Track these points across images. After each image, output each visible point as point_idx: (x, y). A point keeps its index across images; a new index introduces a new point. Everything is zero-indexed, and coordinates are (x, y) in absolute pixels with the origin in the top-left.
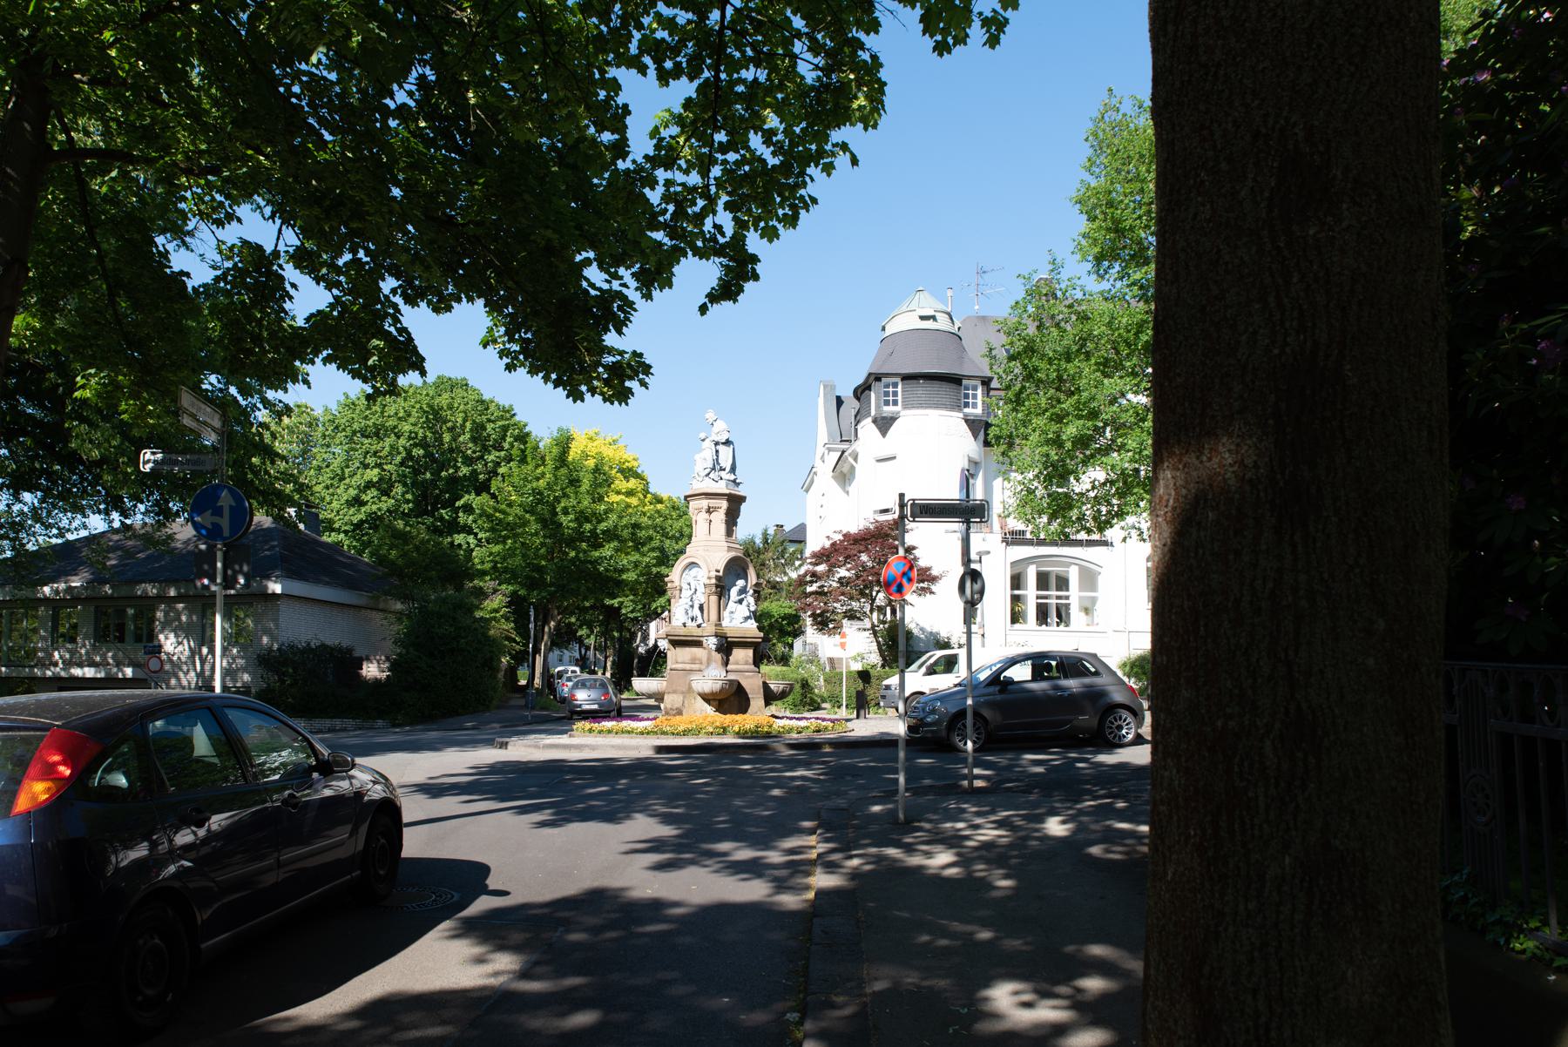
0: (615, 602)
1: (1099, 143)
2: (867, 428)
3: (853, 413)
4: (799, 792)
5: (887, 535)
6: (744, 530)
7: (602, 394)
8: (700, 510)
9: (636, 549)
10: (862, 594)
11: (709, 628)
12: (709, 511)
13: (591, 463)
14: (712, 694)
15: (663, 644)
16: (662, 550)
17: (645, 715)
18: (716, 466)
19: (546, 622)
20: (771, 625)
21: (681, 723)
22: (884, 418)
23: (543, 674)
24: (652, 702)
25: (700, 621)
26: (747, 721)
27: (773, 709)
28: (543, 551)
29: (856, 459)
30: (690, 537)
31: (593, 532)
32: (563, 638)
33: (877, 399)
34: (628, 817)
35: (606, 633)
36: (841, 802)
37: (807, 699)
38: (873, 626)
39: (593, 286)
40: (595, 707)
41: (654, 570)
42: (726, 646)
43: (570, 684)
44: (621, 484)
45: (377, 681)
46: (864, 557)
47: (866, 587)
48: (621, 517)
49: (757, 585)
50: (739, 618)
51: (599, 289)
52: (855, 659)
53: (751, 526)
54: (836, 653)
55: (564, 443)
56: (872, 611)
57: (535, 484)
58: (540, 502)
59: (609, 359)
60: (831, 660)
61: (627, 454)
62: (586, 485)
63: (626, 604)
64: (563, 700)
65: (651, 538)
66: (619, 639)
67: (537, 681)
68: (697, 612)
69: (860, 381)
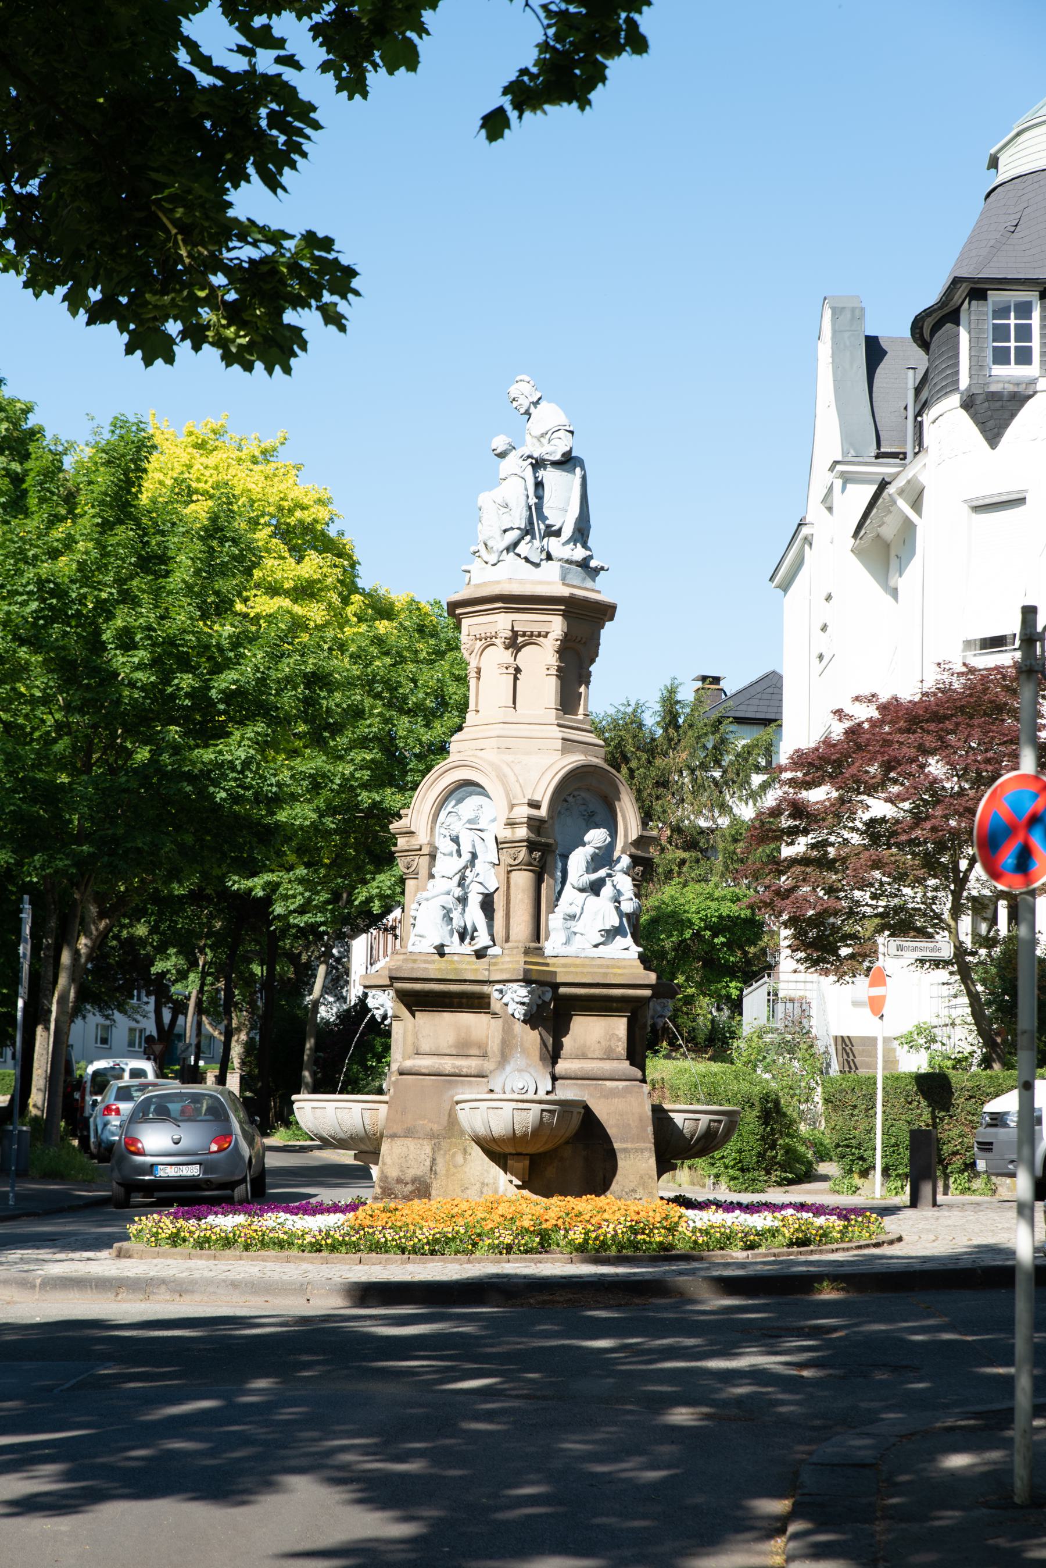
0: (257, 885)
2: (949, 423)
3: (911, 380)
4: (745, 1416)
5: (1000, 708)
6: (607, 693)
7: (221, 343)
8: (488, 641)
9: (317, 740)
10: (931, 865)
11: (508, 960)
12: (515, 643)
13: (199, 511)
14: (514, 1138)
15: (382, 1003)
16: (387, 743)
17: (326, 1195)
18: (535, 524)
19: (65, 938)
20: (682, 948)
21: (423, 1218)
22: (993, 396)
23: (52, 1080)
24: (346, 1157)
25: (483, 939)
26: (607, 1213)
27: (684, 1180)
28: (61, 746)
29: (917, 504)
30: (463, 708)
31: (199, 695)
32: (115, 980)
33: (975, 345)
34: (267, 1484)
35: (229, 968)
36: (858, 1444)
37: (771, 1146)
38: (960, 951)
39: (204, 62)
40: (193, 1171)
41: (365, 798)
42: (554, 1009)
43: (126, 1107)
44: (282, 568)
45: (235, 300)
46: (936, 767)
47: (941, 847)
48: (276, 657)
49: (641, 842)
50: (589, 932)
51: (220, 72)
52: (909, 1041)
53: (627, 681)
54: (858, 1024)
55: (129, 457)
56: (956, 911)
57: (45, 568)
58: (56, 615)
59: (244, 253)
60: (845, 1044)
61: (301, 486)
62: (183, 571)
63: (288, 891)
64: (107, 1152)
65: (357, 713)
66: (268, 983)
67: (37, 1098)
68: (474, 915)
69: (930, 296)
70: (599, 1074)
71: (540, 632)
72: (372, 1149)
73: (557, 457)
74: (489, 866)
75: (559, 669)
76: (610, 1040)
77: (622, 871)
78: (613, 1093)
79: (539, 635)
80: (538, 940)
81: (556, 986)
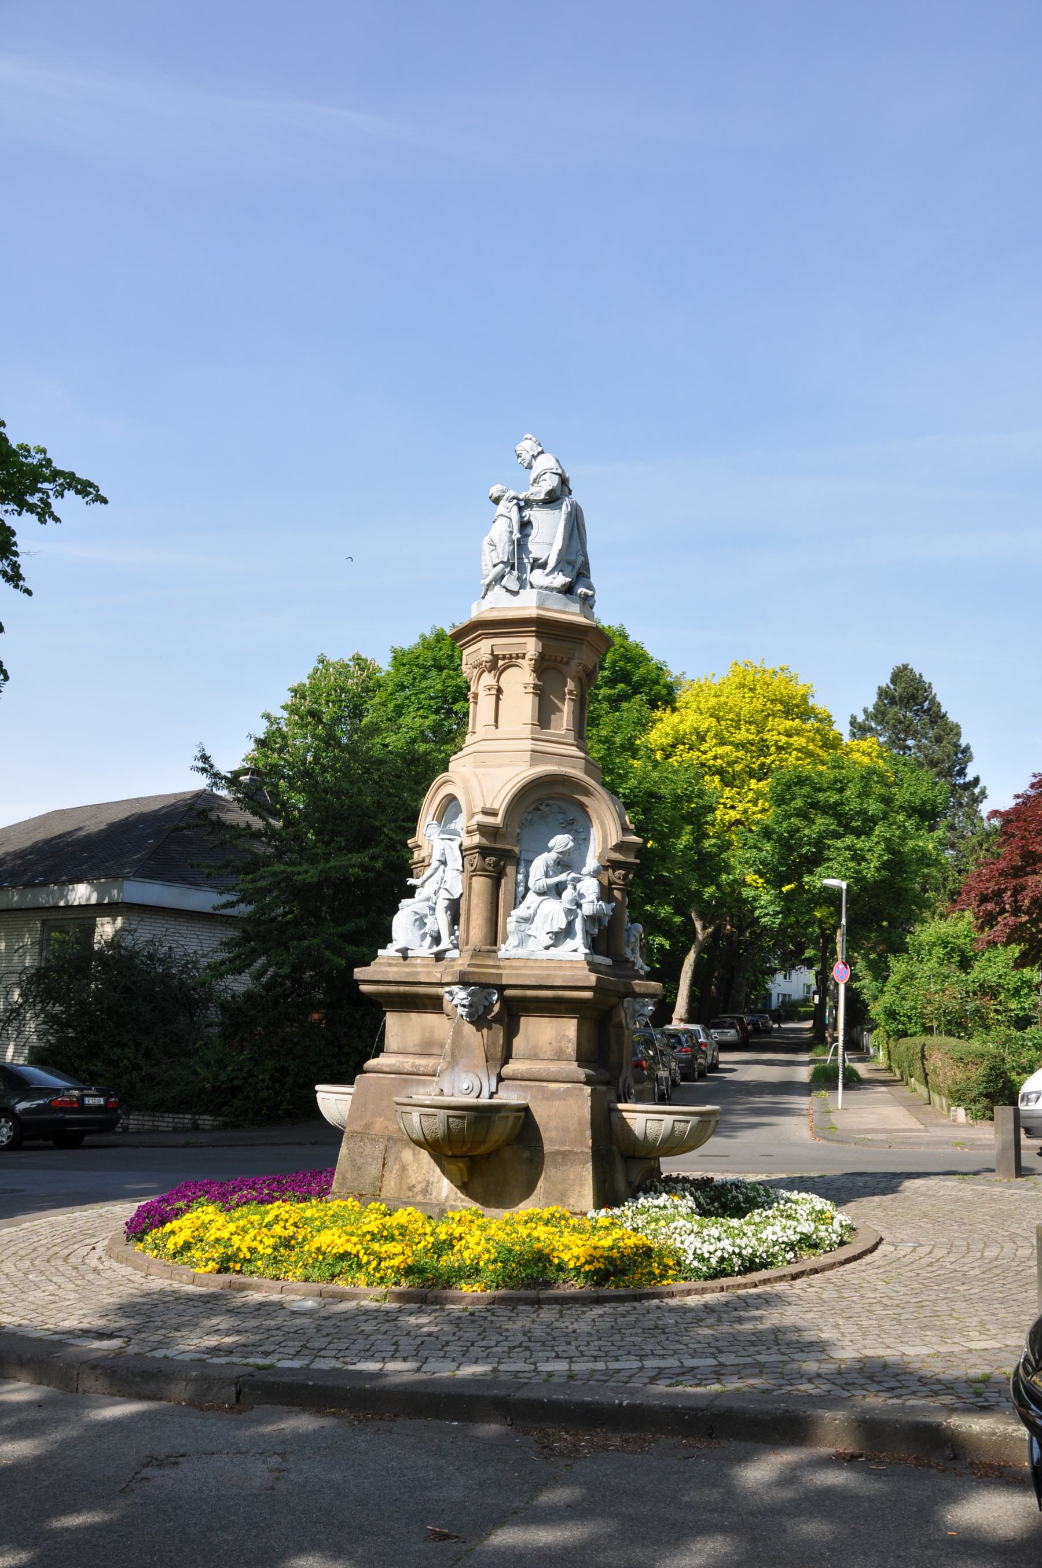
1: (306, 706)
18: (519, 560)
70: (544, 1075)
71: (504, 655)
74: (457, 873)
75: (535, 687)
76: (561, 1041)
77: (589, 874)
78: (554, 1095)
79: (518, 657)
80: (495, 944)
81: (500, 988)
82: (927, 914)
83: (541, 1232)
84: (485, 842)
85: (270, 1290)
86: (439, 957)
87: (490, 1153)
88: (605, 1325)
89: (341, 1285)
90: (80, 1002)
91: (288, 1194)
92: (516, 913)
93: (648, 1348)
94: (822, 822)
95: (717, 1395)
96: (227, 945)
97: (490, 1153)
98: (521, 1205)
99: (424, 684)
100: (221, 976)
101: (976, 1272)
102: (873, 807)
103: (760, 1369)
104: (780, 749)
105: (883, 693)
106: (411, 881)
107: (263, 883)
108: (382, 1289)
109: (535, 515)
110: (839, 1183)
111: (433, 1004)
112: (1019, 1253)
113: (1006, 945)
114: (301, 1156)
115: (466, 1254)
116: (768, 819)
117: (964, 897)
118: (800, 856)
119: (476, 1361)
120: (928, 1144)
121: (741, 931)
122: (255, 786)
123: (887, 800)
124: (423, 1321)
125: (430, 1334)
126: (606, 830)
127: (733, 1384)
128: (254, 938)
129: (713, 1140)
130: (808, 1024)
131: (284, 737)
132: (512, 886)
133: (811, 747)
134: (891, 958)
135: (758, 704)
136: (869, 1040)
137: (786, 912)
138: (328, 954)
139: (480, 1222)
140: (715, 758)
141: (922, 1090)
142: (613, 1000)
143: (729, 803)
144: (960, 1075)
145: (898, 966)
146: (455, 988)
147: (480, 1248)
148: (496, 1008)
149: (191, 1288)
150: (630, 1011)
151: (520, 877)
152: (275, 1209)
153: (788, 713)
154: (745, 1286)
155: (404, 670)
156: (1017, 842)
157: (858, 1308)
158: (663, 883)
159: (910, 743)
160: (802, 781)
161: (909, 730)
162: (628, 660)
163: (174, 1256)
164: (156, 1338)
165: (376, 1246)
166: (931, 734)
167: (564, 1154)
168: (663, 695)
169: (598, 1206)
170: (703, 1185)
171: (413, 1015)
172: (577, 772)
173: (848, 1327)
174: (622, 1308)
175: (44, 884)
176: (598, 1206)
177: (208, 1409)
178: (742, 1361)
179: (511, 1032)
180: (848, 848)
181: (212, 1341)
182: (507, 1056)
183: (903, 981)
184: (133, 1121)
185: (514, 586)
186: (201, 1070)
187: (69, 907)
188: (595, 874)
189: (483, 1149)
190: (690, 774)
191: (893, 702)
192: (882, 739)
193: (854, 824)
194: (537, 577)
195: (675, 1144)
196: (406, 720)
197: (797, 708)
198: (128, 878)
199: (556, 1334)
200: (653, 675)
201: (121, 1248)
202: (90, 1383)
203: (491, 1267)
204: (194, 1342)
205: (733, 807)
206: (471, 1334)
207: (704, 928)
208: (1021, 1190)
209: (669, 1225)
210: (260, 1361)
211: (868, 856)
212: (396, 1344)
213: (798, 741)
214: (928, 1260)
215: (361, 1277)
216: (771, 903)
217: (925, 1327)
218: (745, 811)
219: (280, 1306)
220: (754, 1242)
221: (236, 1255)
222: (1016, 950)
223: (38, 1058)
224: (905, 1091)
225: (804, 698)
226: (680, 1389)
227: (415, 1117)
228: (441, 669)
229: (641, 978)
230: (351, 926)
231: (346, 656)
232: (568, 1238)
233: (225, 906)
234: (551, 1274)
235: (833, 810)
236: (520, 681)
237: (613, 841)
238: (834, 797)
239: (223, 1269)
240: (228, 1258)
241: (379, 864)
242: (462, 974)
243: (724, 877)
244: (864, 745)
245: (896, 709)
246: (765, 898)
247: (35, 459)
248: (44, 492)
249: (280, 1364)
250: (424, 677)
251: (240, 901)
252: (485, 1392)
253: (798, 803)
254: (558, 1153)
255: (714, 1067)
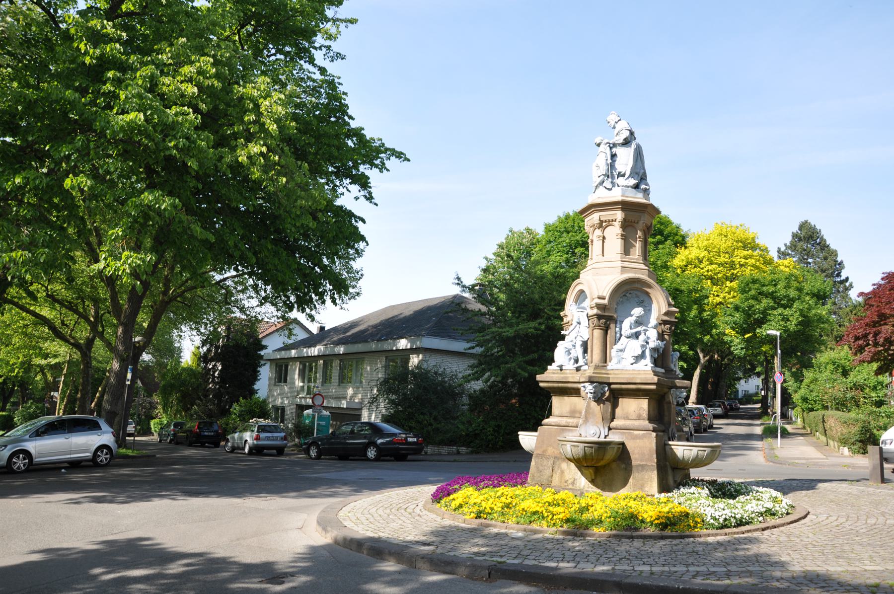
1: (506, 253)
18: (611, 173)
70: (632, 427)
72: (886, 476)
73: (621, 141)
75: (622, 235)
81: (609, 384)
82: (823, 348)
83: (632, 504)
84: (599, 312)
85: (501, 527)
86: (578, 369)
87: (605, 464)
88: (667, 549)
89: (535, 526)
90: (404, 394)
91: (507, 483)
92: (616, 347)
93: (690, 561)
94: (766, 302)
95: (729, 586)
96: (471, 367)
97: (605, 464)
98: (621, 491)
99: (561, 240)
100: (469, 381)
101: (864, 530)
102: (793, 293)
103: (751, 574)
104: (741, 266)
105: (794, 236)
106: (563, 332)
107: (488, 337)
108: (554, 529)
109: (618, 151)
110: (782, 484)
111: (576, 392)
112: (888, 522)
113: (869, 362)
114: (513, 464)
115: (595, 513)
116: (737, 301)
117: (846, 337)
118: (754, 319)
119: (604, 564)
120: (829, 466)
121: (723, 359)
122: (481, 291)
123: (800, 290)
124: (576, 544)
125: (580, 551)
126: (660, 305)
127: (736, 581)
128: (484, 363)
129: (716, 463)
130: (759, 406)
131: (495, 268)
132: (613, 334)
133: (758, 264)
134: (804, 371)
135: (729, 243)
136: (792, 413)
137: (747, 348)
138: (519, 371)
139: (601, 498)
140: (708, 271)
141: (823, 438)
142: (666, 390)
143: (716, 293)
144: (845, 431)
145: (808, 375)
146: (587, 384)
147: (602, 511)
148: (607, 394)
149: (463, 525)
150: (674, 396)
151: (617, 329)
152: (501, 490)
153: (745, 247)
154: (738, 533)
155: (550, 234)
156: (874, 309)
157: (800, 546)
158: (687, 332)
159: (810, 260)
160: (754, 281)
161: (809, 254)
162: (662, 224)
163: (455, 510)
164: (450, 546)
165: (551, 508)
166: (821, 255)
167: (643, 466)
168: (681, 242)
169: (660, 492)
170: (712, 483)
171: (566, 398)
172: (644, 277)
173: (795, 555)
174: (675, 542)
175: (386, 340)
176: (660, 492)
177: (476, 580)
178: (740, 569)
179: (615, 406)
180: (780, 315)
181: (476, 549)
182: (613, 418)
183: (811, 382)
184: (429, 449)
185: (610, 186)
186: (461, 427)
187: (397, 350)
188: (655, 327)
189: (602, 463)
190: (696, 279)
191: (800, 240)
192: (795, 259)
193: (782, 302)
194: (621, 181)
195: (698, 462)
196: (552, 258)
197: (749, 245)
198: (423, 336)
199: (642, 553)
200: (675, 231)
201: (430, 506)
202: (420, 564)
203: (608, 520)
204: (468, 549)
205: (718, 296)
206: (601, 552)
207: (704, 357)
208: (884, 491)
209: (695, 501)
210: (499, 560)
211: (791, 318)
212: (563, 554)
213: (751, 261)
214: (835, 523)
215: (544, 523)
216: (740, 343)
217: (838, 557)
218: (724, 298)
219: (506, 535)
220: (742, 511)
221: (484, 511)
222: (875, 366)
223: (386, 419)
224: (814, 439)
225: (753, 239)
226: (709, 581)
227: (568, 446)
228: (568, 232)
229: (679, 379)
230: (530, 357)
231: (522, 229)
232: (646, 507)
233: (470, 348)
234: (638, 524)
235: (771, 295)
236: (614, 233)
237: (664, 310)
238: (772, 289)
239: (478, 517)
240: (480, 512)
241: (543, 327)
242: (590, 377)
243: (714, 331)
244: (786, 262)
245: (802, 243)
246: (736, 341)
247: (377, 144)
248: (382, 158)
249: (508, 561)
250: (560, 237)
251: (477, 346)
252: (610, 579)
253: (753, 292)
254: (640, 465)
255: (711, 427)
